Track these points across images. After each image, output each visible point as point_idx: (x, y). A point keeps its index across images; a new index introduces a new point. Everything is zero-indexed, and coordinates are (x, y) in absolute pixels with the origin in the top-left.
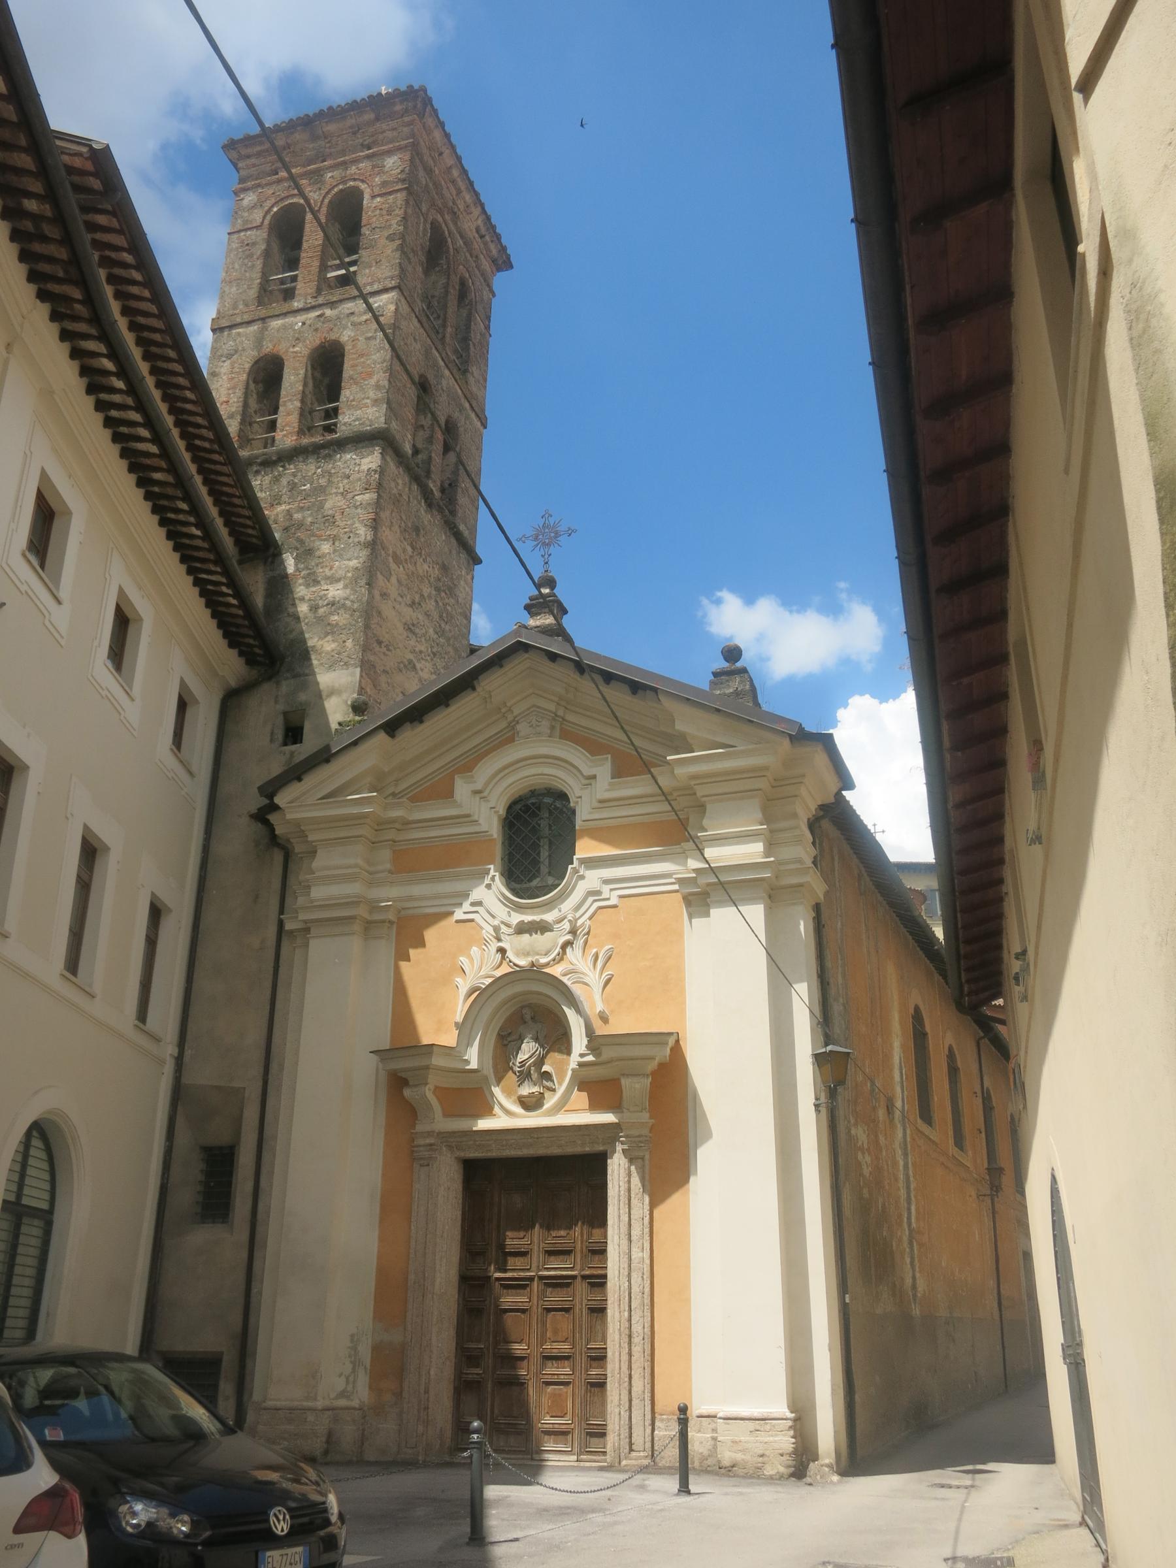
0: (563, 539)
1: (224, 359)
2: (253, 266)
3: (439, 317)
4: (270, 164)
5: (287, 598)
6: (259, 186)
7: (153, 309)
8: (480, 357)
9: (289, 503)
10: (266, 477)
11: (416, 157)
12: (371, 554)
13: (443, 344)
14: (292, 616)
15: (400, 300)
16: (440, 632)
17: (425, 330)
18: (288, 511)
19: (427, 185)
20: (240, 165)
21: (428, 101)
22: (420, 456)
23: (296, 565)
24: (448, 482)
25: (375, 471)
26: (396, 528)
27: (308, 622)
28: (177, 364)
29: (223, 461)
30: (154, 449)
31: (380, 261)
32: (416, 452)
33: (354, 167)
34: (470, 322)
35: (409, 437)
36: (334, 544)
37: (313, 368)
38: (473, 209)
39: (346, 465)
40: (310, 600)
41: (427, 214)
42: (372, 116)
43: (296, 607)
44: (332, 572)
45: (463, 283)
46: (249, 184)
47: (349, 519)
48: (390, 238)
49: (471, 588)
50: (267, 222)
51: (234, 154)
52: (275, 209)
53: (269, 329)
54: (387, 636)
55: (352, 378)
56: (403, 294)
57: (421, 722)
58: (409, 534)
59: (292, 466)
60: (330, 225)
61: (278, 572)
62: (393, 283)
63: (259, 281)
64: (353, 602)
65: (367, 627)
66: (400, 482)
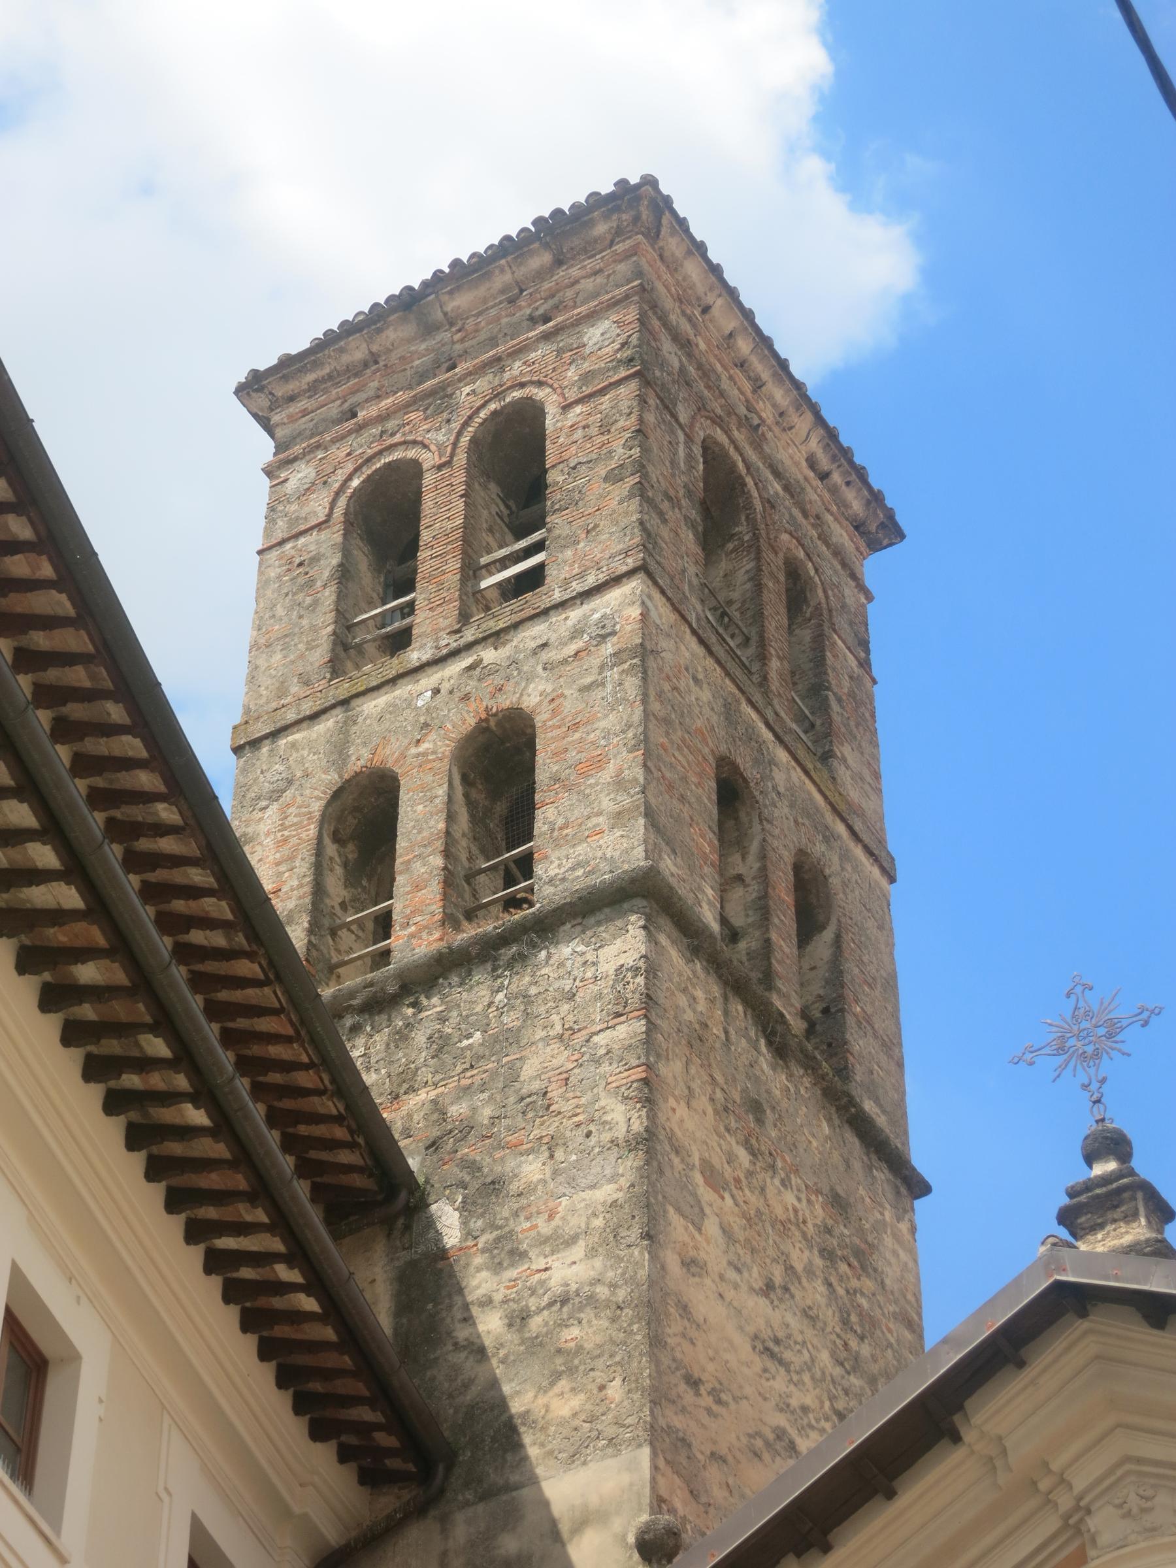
0: (1132, 1036)
1: (264, 803)
2: (316, 603)
3: (747, 640)
4: (338, 402)
5: (450, 1307)
6: (318, 446)
7: (60, 603)
8: (858, 725)
9: (436, 1085)
10: (377, 1037)
11: (650, 313)
12: (647, 1163)
13: (766, 693)
14: (465, 1347)
15: (649, 597)
16: (851, 1363)
17: (718, 662)
18: (435, 1102)
19: (682, 370)
20: (276, 418)
21: (663, 205)
22: (742, 945)
23: (465, 1223)
24: (820, 1006)
25: (636, 970)
26: (703, 1102)
27: (507, 1356)
28: (130, 737)
29: (262, 977)
30: (69, 897)
31: (596, 526)
32: (733, 936)
33: (518, 364)
34: (823, 651)
35: (710, 892)
36: (552, 1157)
37: (465, 779)
38: (794, 418)
39: (562, 971)
40: (505, 1301)
41: (692, 426)
42: (546, 258)
43: (474, 1324)
44: (554, 1223)
45: (793, 572)
46: (297, 449)
47: (584, 1093)
48: (613, 477)
49: (912, 1253)
50: (339, 511)
51: (262, 401)
52: (355, 483)
53: (360, 719)
54: (711, 1367)
55: (557, 780)
56: (656, 583)
57: (826, 1548)
58: (739, 1118)
59: (435, 1000)
60: (477, 486)
61: (421, 1249)
62: (631, 563)
63: (330, 629)
64: (613, 1286)
65: (656, 1342)
66: (699, 994)
